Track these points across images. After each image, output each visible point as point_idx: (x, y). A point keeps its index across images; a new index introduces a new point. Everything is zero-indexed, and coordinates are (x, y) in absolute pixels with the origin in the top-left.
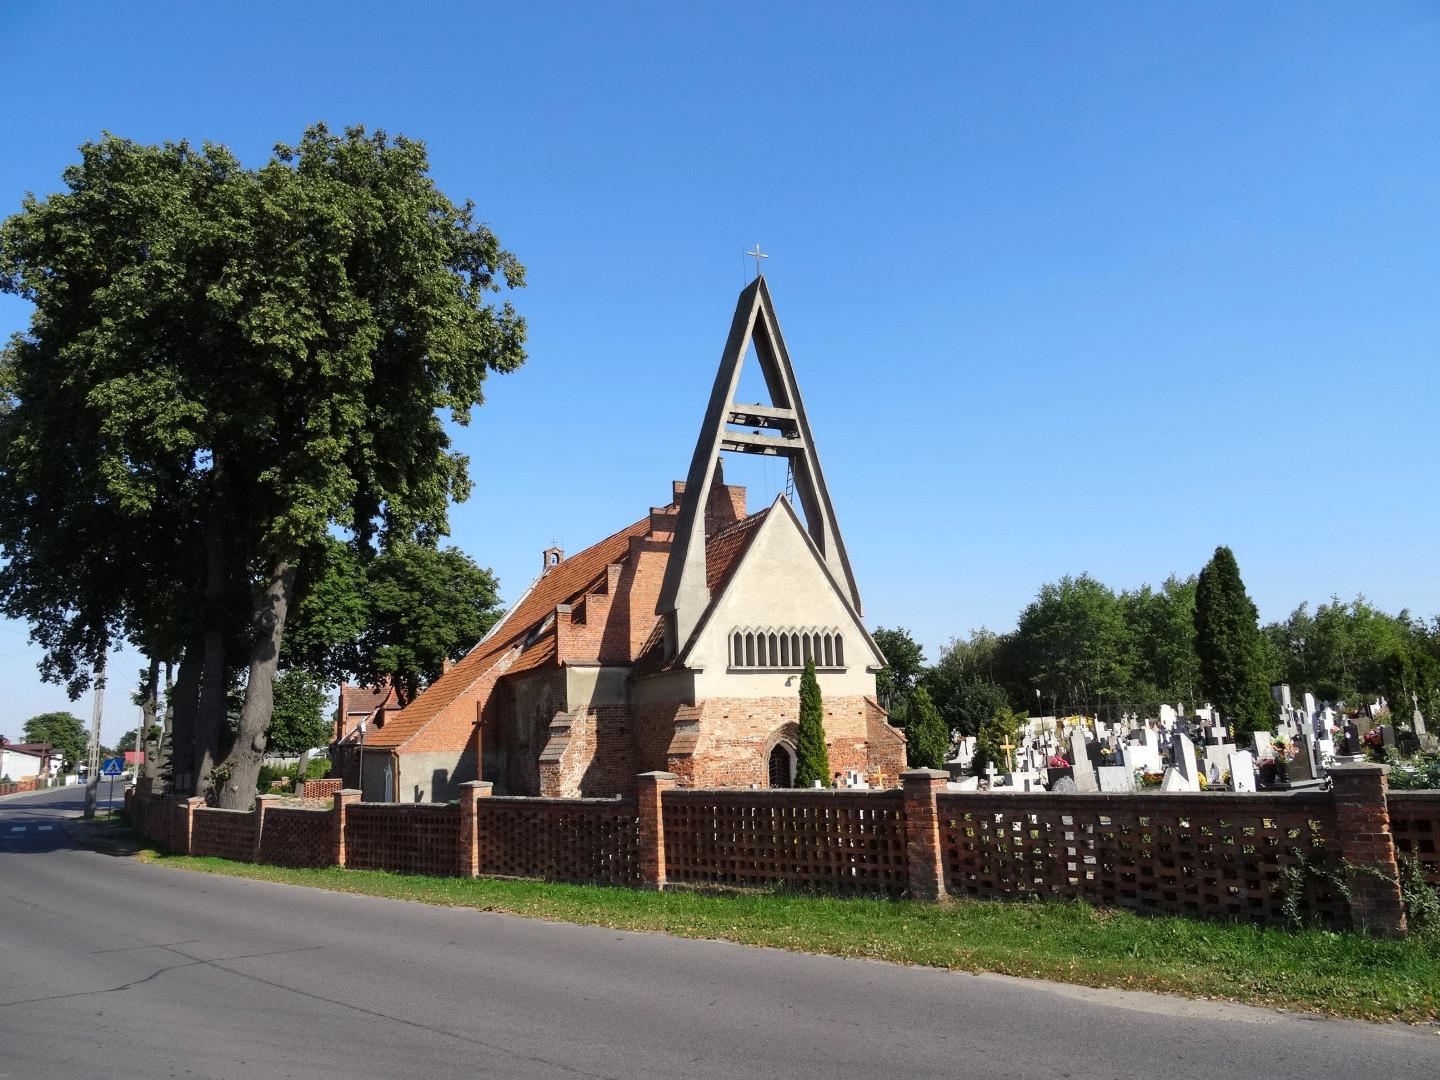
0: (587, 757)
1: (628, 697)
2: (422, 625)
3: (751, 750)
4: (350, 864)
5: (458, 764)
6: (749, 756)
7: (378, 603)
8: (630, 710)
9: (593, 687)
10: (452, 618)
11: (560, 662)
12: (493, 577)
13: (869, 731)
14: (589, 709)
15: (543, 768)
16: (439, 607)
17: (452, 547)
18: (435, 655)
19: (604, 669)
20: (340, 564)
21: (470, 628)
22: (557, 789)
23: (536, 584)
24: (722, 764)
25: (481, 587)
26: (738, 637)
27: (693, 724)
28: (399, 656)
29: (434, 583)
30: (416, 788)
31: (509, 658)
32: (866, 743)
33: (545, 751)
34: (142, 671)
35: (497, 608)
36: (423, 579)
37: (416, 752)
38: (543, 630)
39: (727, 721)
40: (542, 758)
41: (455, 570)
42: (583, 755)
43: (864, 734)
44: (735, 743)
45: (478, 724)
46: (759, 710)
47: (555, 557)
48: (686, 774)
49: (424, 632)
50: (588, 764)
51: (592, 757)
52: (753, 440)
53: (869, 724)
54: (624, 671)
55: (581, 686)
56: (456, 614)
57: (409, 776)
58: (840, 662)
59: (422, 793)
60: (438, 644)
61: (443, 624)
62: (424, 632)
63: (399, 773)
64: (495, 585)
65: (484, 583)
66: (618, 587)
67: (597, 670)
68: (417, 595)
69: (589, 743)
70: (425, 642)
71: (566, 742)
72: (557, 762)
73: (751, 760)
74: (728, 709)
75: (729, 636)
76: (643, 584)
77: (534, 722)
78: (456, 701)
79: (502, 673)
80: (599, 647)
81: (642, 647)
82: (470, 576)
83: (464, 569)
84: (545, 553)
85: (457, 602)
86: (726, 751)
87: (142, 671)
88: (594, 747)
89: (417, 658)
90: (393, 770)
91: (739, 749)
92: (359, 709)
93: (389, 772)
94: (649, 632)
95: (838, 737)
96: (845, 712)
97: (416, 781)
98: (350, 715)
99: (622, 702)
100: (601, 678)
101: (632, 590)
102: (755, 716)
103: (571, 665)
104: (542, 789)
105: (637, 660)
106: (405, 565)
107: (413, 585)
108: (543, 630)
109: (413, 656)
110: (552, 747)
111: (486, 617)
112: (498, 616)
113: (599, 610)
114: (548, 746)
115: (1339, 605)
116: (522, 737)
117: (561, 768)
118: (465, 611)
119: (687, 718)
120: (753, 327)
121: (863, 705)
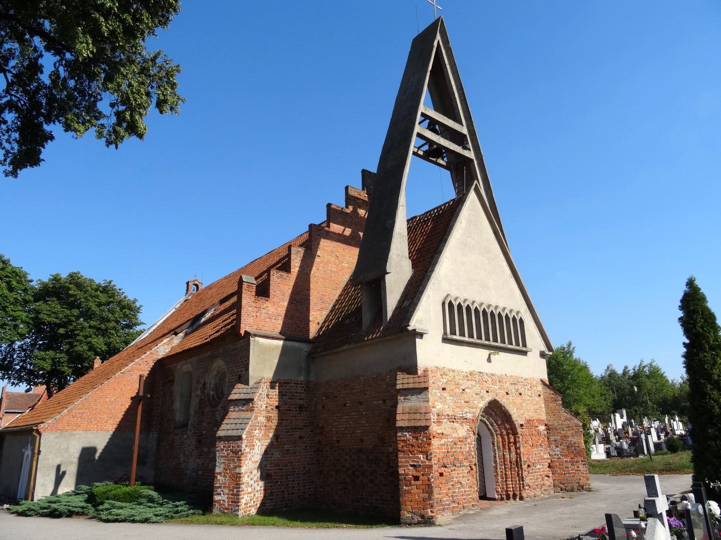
0: (266, 435)
1: (308, 372)
2: (78, 335)
5: (108, 443)
7: (41, 316)
8: (309, 387)
9: (276, 361)
10: (104, 333)
11: (242, 332)
12: (138, 304)
13: (547, 413)
14: (271, 383)
15: (221, 445)
16: (93, 323)
17: (108, 280)
18: (86, 359)
19: (290, 343)
20: (11, 281)
21: (115, 340)
22: (237, 470)
23: (179, 305)
24: (442, 442)
25: (129, 310)
26: (451, 305)
27: (420, 393)
28: (53, 359)
29: (91, 304)
30: (59, 467)
31: (168, 343)
32: (546, 425)
33: (223, 427)
35: (138, 328)
36: (83, 300)
37: (62, 430)
38: (203, 320)
39: (445, 394)
40: (220, 433)
41: (110, 297)
42: (263, 432)
43: (544, 417)
44: (453, 419)
45: (136, 400)
46: (469, 383)
47: (195, 287)
48: (421, 452)
49: (78, 341)
50: (267, 442)
51: (271, 435)
52: (439, 141)
53: (547, 406)
54: (305, 347)
55: (265, 358)
56: (106, 330)
57: (50, 457)
58: (525, 345)
59: (64, 473)
60: (89, 350)
61: (93, 336)
62: (78, 341)
63: (39, 452)
64: (138, 310)
65: (130, 308)
66: (301, 267)
67: (281, 343)
68: (76, 312)
69: (269, 419)
70: (79, 348)
71: (248, 416)
72: (240, 438)
73: (466, 438)
74: (445, 380)
75: (443, 304)
76: (321, 268)
77: (197, 400)
78: (112, 380)
79: (160, 357)
80: (281, 322)
81: (319, 327)
82: (120, 302)
83: (116, 298)
84: (188, 283)
85: (109, 321)
87: (58, 275)
88: (275, 422)
89: (69, 361)
90: (33, 450)
91: (456, 425)
92: (15, 409)
93: (28, 452)
94: (325, 313)
97: (57, 461)
98: (6, 413)
99: (302, 378)
100: (284, 352)
101: (312, 272)
102: (467, 390)
103: (255, 335)
104: (218, 470)
105: (314, 338)
106: (69, 289)
107: (73, 305)
108: (203, 320)
109: (66, 359)
110: (231, 421)
111: (132, 334)
112: (140, 333)
113: (282, 286)
114: (226, 421)
115: (643, 365)
116: (179, 417)
117: (243, 446)
118: (114, 328)
119: (411, 386)
120: (428, 69)
121: (540, 388)
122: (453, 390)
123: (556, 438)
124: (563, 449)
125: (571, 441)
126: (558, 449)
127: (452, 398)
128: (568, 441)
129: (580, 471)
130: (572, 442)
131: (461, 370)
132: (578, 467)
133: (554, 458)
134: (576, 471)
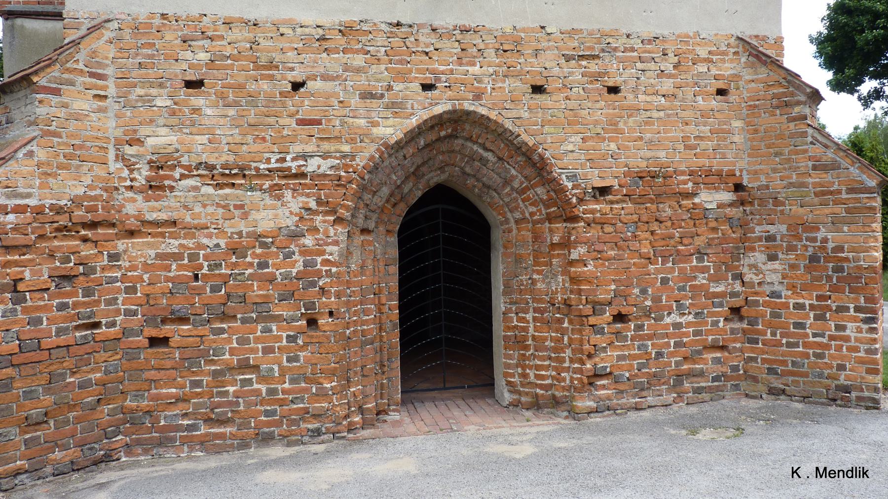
3: (294, 203)
4: (876, 323)
6: (291, 222)
24: (173, 245)
32: (738, 187)
34: (810, 36)
39: (198, 100)
44: (226, 176)
46: (331, 63)
73: (295, 236)
74: (203, 56)
86: (190, 198)
87: (810, 36)
95: (639, 159)
96: (667, 85)
122: (241, 87)
123: (772, 229)
124: (793, 267)
125: (825, 240)
126: (776, 265)
127: (232, 112)
128: (814, 240)
129: (847, 339)
130: (830, 245)
131: (286, 22)
132: (843, 328)
133: (756, 294)
134: (832, 338)
